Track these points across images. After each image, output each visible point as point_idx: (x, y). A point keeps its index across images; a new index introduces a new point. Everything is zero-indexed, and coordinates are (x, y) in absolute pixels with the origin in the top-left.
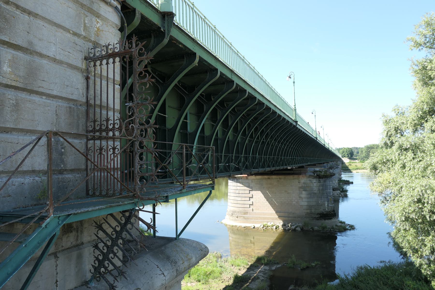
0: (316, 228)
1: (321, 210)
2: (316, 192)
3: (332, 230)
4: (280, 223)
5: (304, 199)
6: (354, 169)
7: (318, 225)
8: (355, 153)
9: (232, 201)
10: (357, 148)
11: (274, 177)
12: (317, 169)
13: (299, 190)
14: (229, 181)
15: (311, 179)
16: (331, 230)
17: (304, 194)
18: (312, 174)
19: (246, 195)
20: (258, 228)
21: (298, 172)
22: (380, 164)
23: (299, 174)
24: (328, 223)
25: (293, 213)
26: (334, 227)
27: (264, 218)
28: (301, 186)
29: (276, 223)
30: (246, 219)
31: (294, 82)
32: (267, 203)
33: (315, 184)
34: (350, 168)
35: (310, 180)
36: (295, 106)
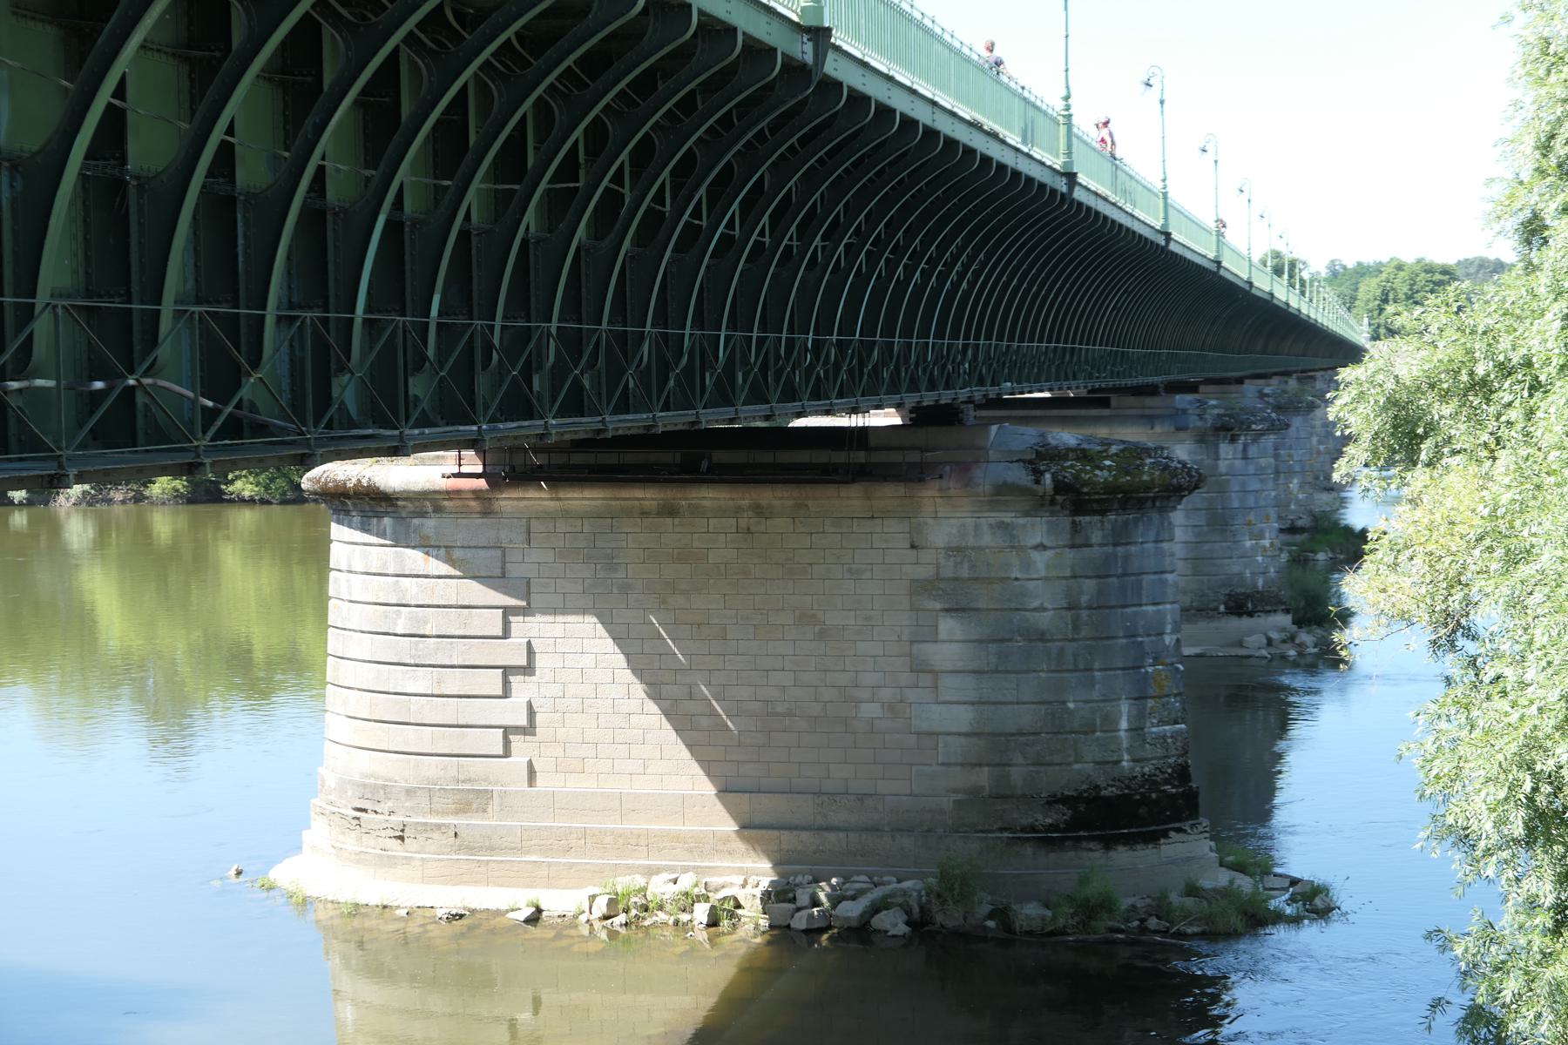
0: (1030, 913)
1: (1081, 768)
2: (1045, 620)
3: (1153, 923)
4: (747, 877)
5: (947, 682)
9: (362, 704)
11: (710, 496)
12: (1066, 437)
13: (921, 615)
14: (338, 531)
15: (1007, 517)
16: (1143, 929)
17: (951, 644)
18: (1019, 475)
20: (568, 922)
21: (896, 457)
22: (1445, 396)
23: (915, 474)
24: (1132, 873)
25: (862, 797)
26: (1175, 898)
27: (628, 842)
28: (925, 572)
29: (715, 880)
30: (470, 849)
32: (652, 718)
33: (1040, 560)
35: (1003, 527)
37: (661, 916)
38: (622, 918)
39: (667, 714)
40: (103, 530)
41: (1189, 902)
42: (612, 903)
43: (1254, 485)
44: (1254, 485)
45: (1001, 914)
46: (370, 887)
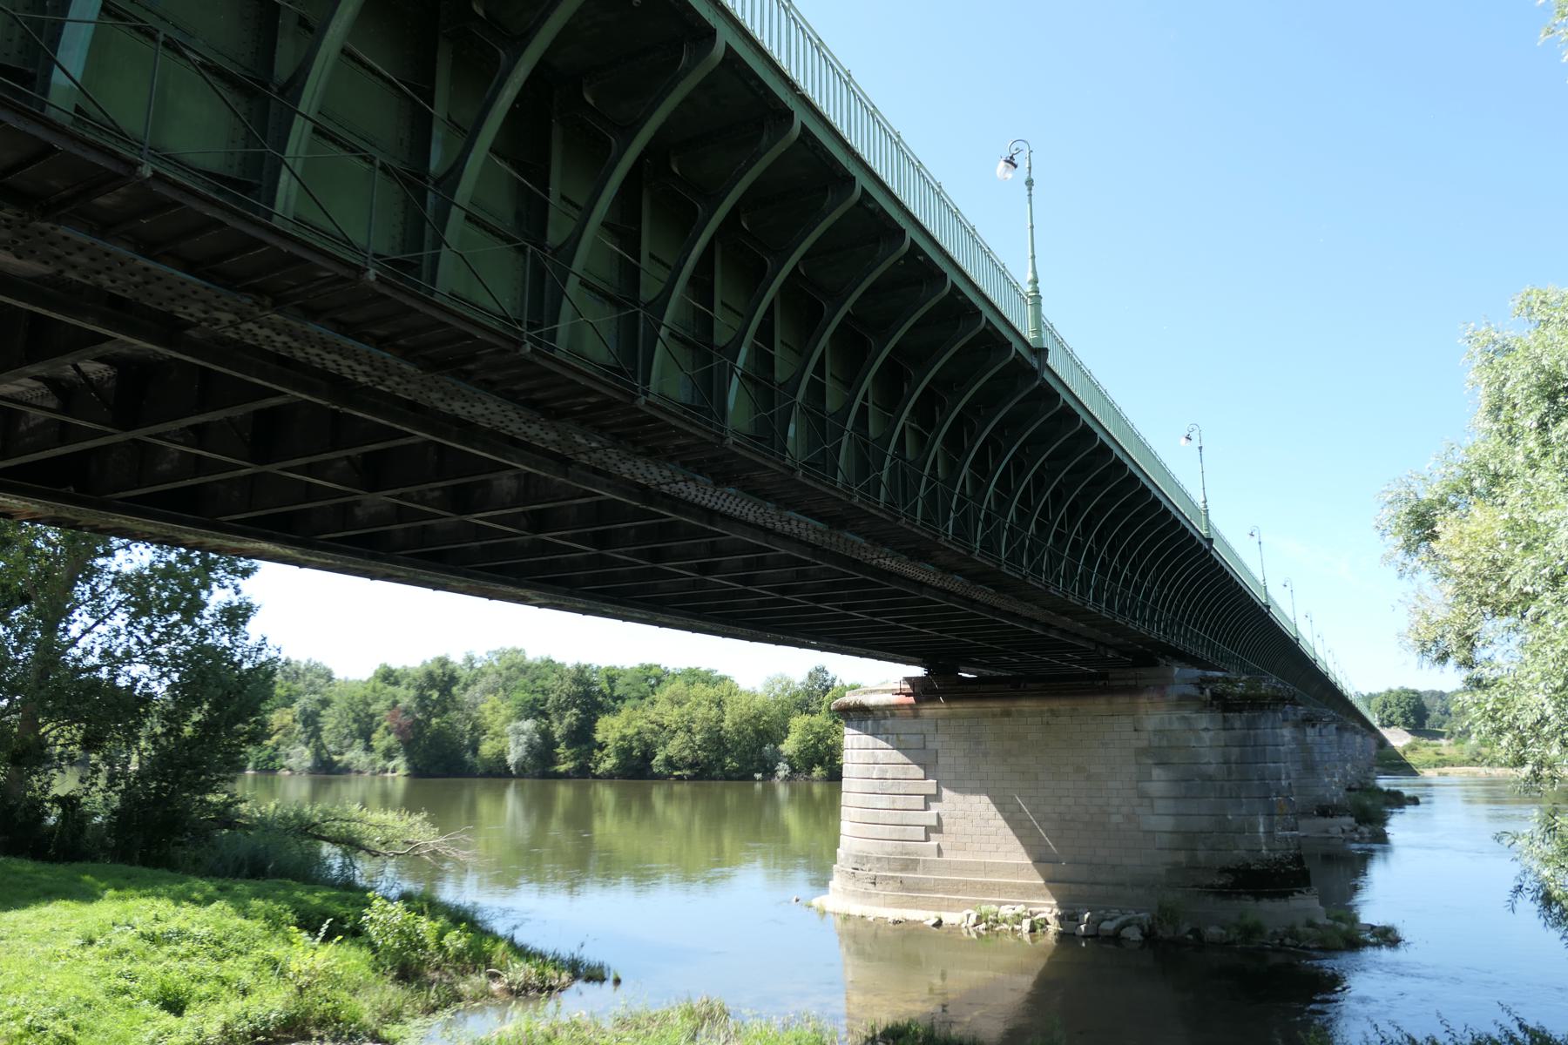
0: (1213, 931)
1: (1239, 853)
2: (1211, 769)
3: (1288, 941)
4: (1048, 909)
5: (1159, 804)
6: (1428, 765)
7: (1221, 919)
8: (1435, 715)
10: (1442, 695)
11: (1027, 705)
13: (1139, 760)
14: (847, 730)
15: (1186, 713)
16: (1282, 943)
17: (1159, 782)
18: (1194, 691)
19: (912, 787)
20: (955, 928)
24: (1274, 914)
25: (1114, 866)
26: (1300, 929)
27: (988, 888)
28: (1145, 743)
29: (1035, 910)
30: (908, 890)
31: (1030, 183)
32: (1000, 822)
33: (1206, 735)
34: (1412, 758)
36: (1035, 281)
37: (1005, 926)
38: (983, 925)
39: (1006, 819)
40: (793, 792)
41: (1310, 930)
43: (1326, 749)
44: (1326, 749)
45: (1194, 931)
46: (856, 909)
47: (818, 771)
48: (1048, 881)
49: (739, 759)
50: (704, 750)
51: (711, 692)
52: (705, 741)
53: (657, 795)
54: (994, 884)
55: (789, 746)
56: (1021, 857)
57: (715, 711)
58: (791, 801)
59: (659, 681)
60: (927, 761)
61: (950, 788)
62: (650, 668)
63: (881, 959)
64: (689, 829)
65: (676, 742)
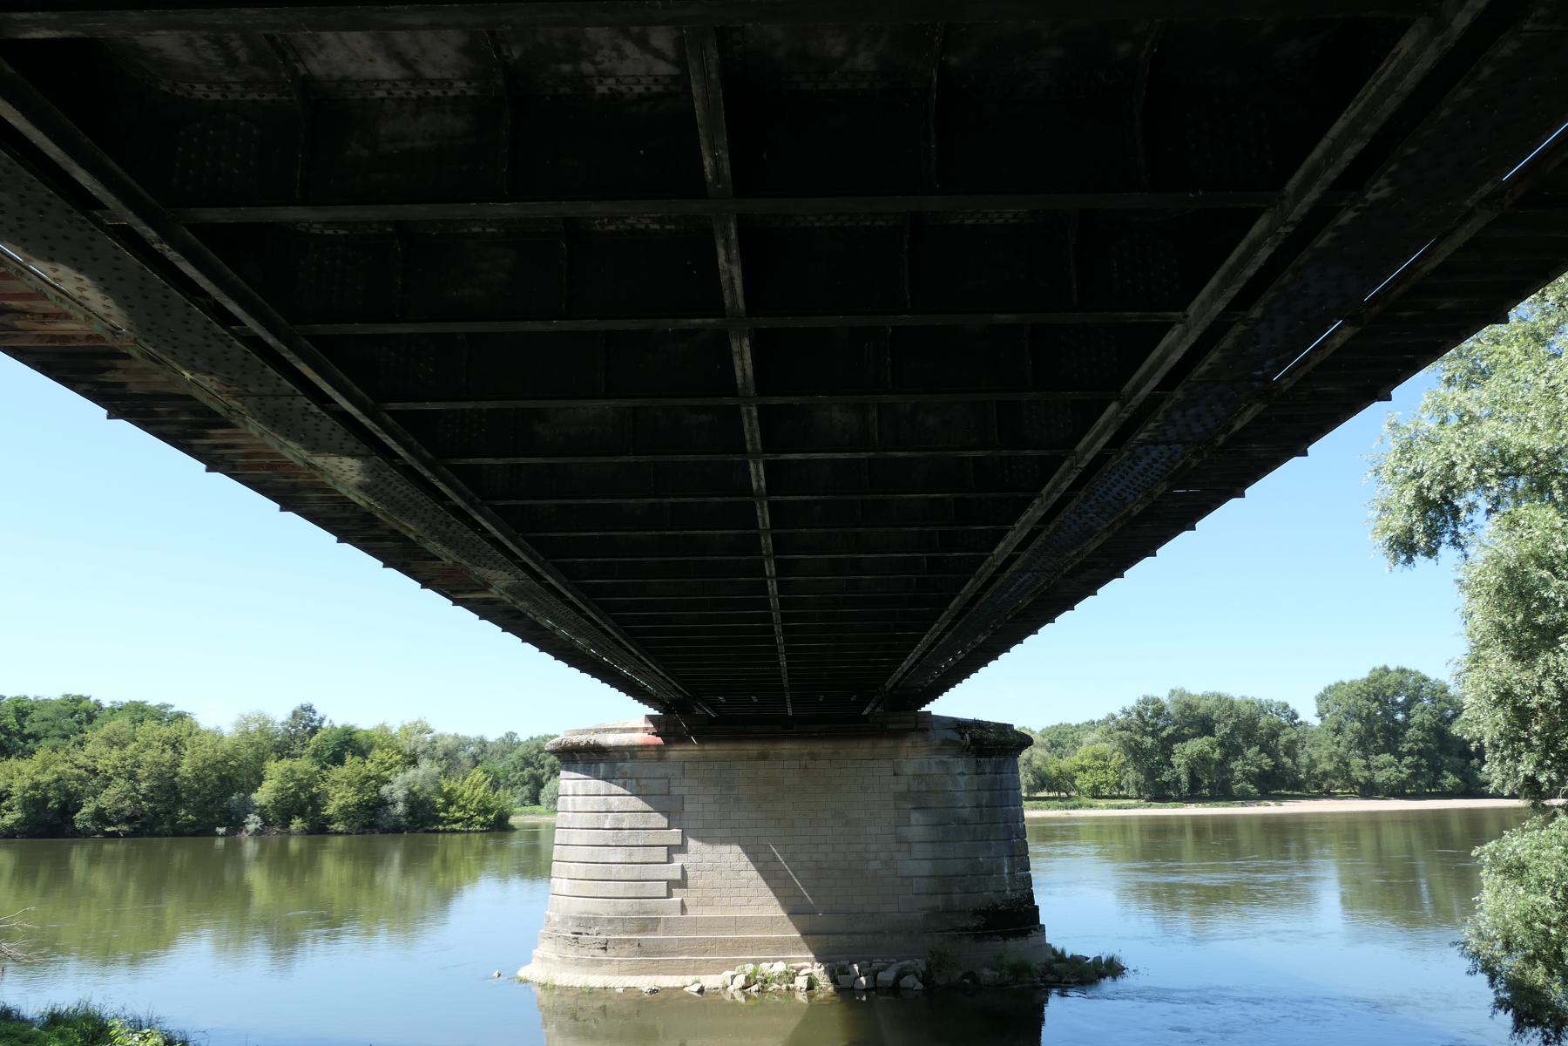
2: (966, 813)
9: (580, 870)
11: (787, 748)
15: (944, 758)
17: (918, 826)
28: (902, 788)
30: (647, 954)
38: (755, 988)
39: (759, 870)
40: (262, 851)
42: (747, 978)
47: (297, 824)
48: (802, 935)
49: (198, 811)
50: (151, 800)
51: (166, 731)
52: (151, 789)
53: (78, 859)
54: (747, 941)
55: (263, 795)
56: (774, 910)
57: (169, 753)
58: (259, 858)
59: (91, 718)
60: (669, 806)
61: (696, 838)
62: (79, 700)
63: (608, 1036)
64: (119, 896)
65: (111, 791)
